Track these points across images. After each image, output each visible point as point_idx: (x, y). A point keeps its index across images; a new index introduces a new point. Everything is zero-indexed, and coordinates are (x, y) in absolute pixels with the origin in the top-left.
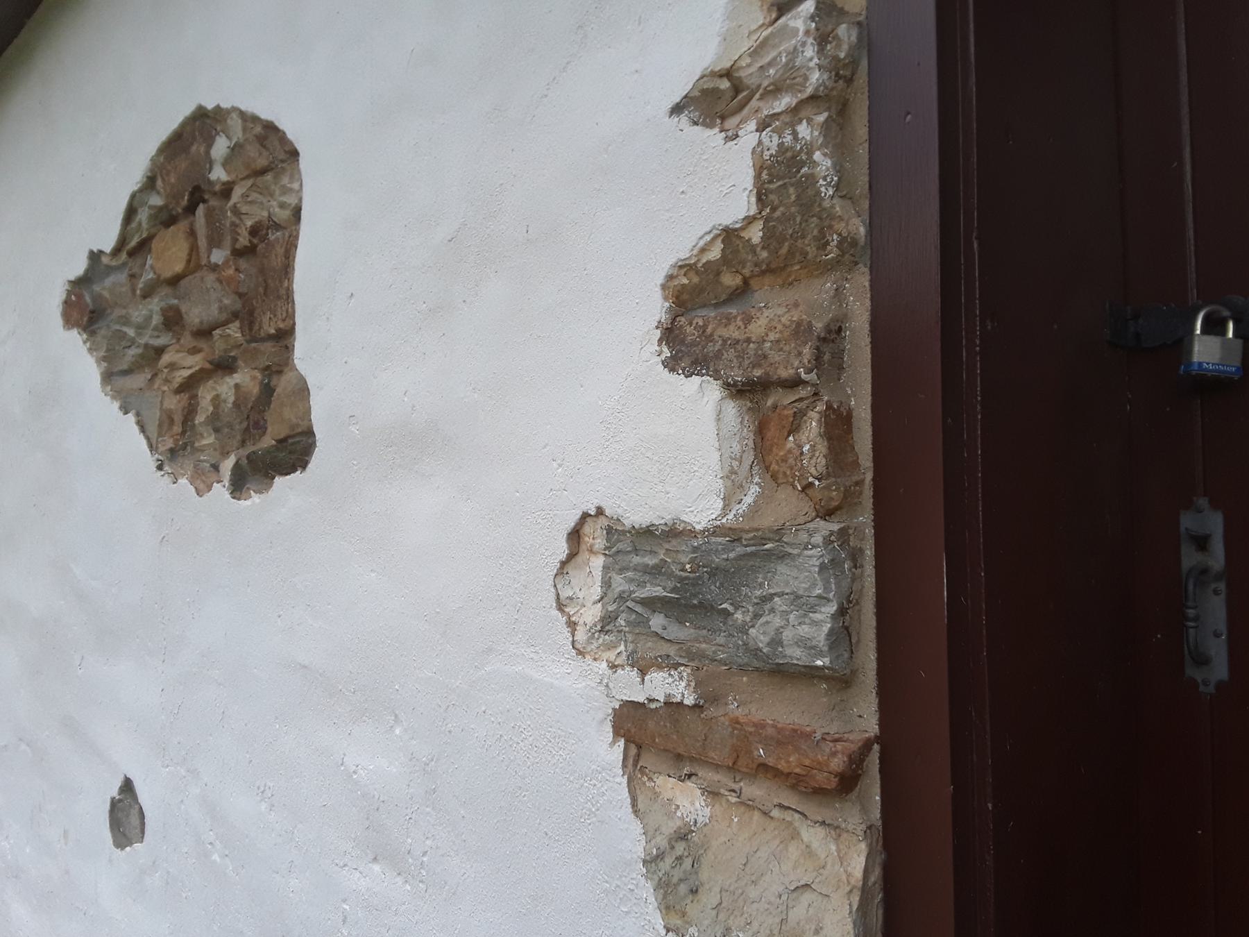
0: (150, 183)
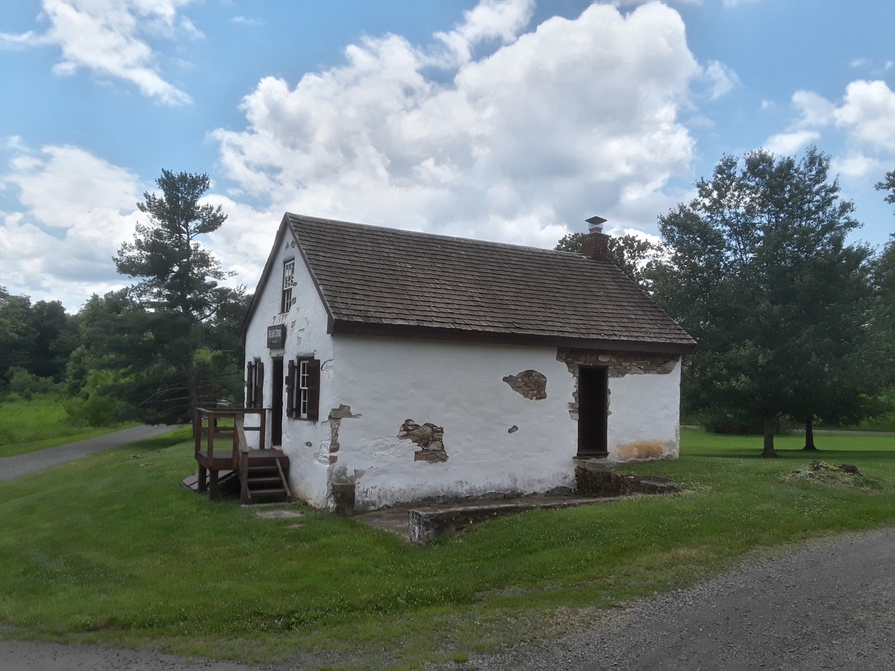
0: (523, 373)
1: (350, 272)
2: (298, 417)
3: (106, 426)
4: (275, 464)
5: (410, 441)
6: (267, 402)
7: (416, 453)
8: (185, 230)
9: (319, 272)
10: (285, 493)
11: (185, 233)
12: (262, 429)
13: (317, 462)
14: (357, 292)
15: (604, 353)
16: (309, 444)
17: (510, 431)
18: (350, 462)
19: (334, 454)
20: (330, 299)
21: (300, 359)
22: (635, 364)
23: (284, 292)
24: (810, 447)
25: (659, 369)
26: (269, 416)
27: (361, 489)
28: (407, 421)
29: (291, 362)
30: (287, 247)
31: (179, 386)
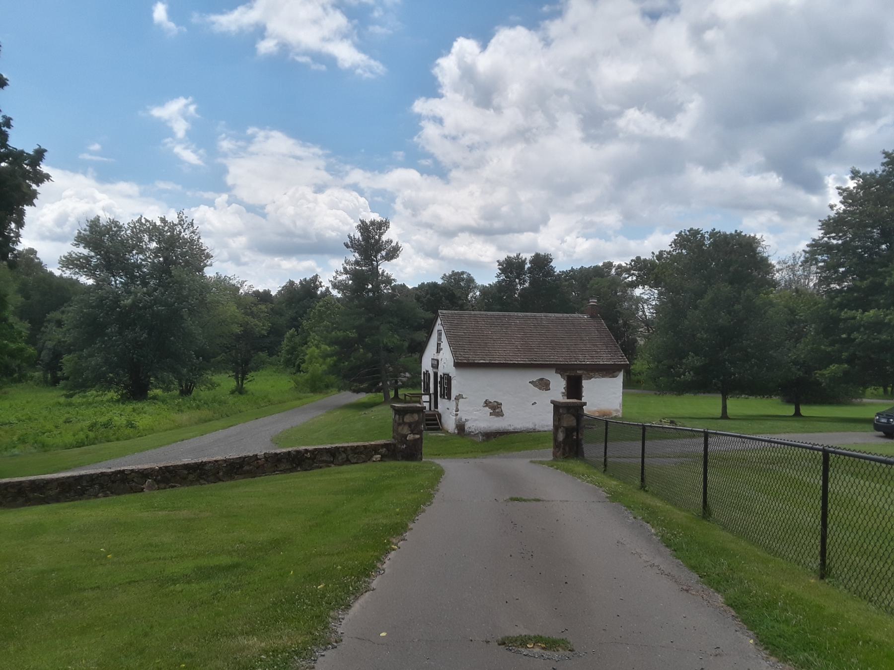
1: (464, 339)
2: (444, 398)
3: (321, 392)
4: (435, 416)
5: (487, 408)
6: (432, 391)
7: (490, 413)
8: (375, 259)
9: (451, 340)
10: (440, 427)
11: (374, 261)
12: (430, 402)
13: (451, 416)
14: (465, 348)
15: (580, 369)
16: (448, 409)
17: (533, 404)
18: (463, 416)
19: (457, 413)
20: (454, 353)
21: (444, 375)
22: (597, 373)
23: (438, 344)
24: (797, 414)
25: (611, 376)
26: (433, 396)
27: (468, 426)
28: (486, 400)
29: (441, 375)
30: (439, 325)
31: (374, 367)
